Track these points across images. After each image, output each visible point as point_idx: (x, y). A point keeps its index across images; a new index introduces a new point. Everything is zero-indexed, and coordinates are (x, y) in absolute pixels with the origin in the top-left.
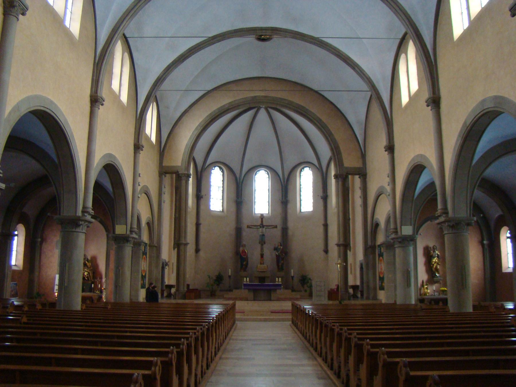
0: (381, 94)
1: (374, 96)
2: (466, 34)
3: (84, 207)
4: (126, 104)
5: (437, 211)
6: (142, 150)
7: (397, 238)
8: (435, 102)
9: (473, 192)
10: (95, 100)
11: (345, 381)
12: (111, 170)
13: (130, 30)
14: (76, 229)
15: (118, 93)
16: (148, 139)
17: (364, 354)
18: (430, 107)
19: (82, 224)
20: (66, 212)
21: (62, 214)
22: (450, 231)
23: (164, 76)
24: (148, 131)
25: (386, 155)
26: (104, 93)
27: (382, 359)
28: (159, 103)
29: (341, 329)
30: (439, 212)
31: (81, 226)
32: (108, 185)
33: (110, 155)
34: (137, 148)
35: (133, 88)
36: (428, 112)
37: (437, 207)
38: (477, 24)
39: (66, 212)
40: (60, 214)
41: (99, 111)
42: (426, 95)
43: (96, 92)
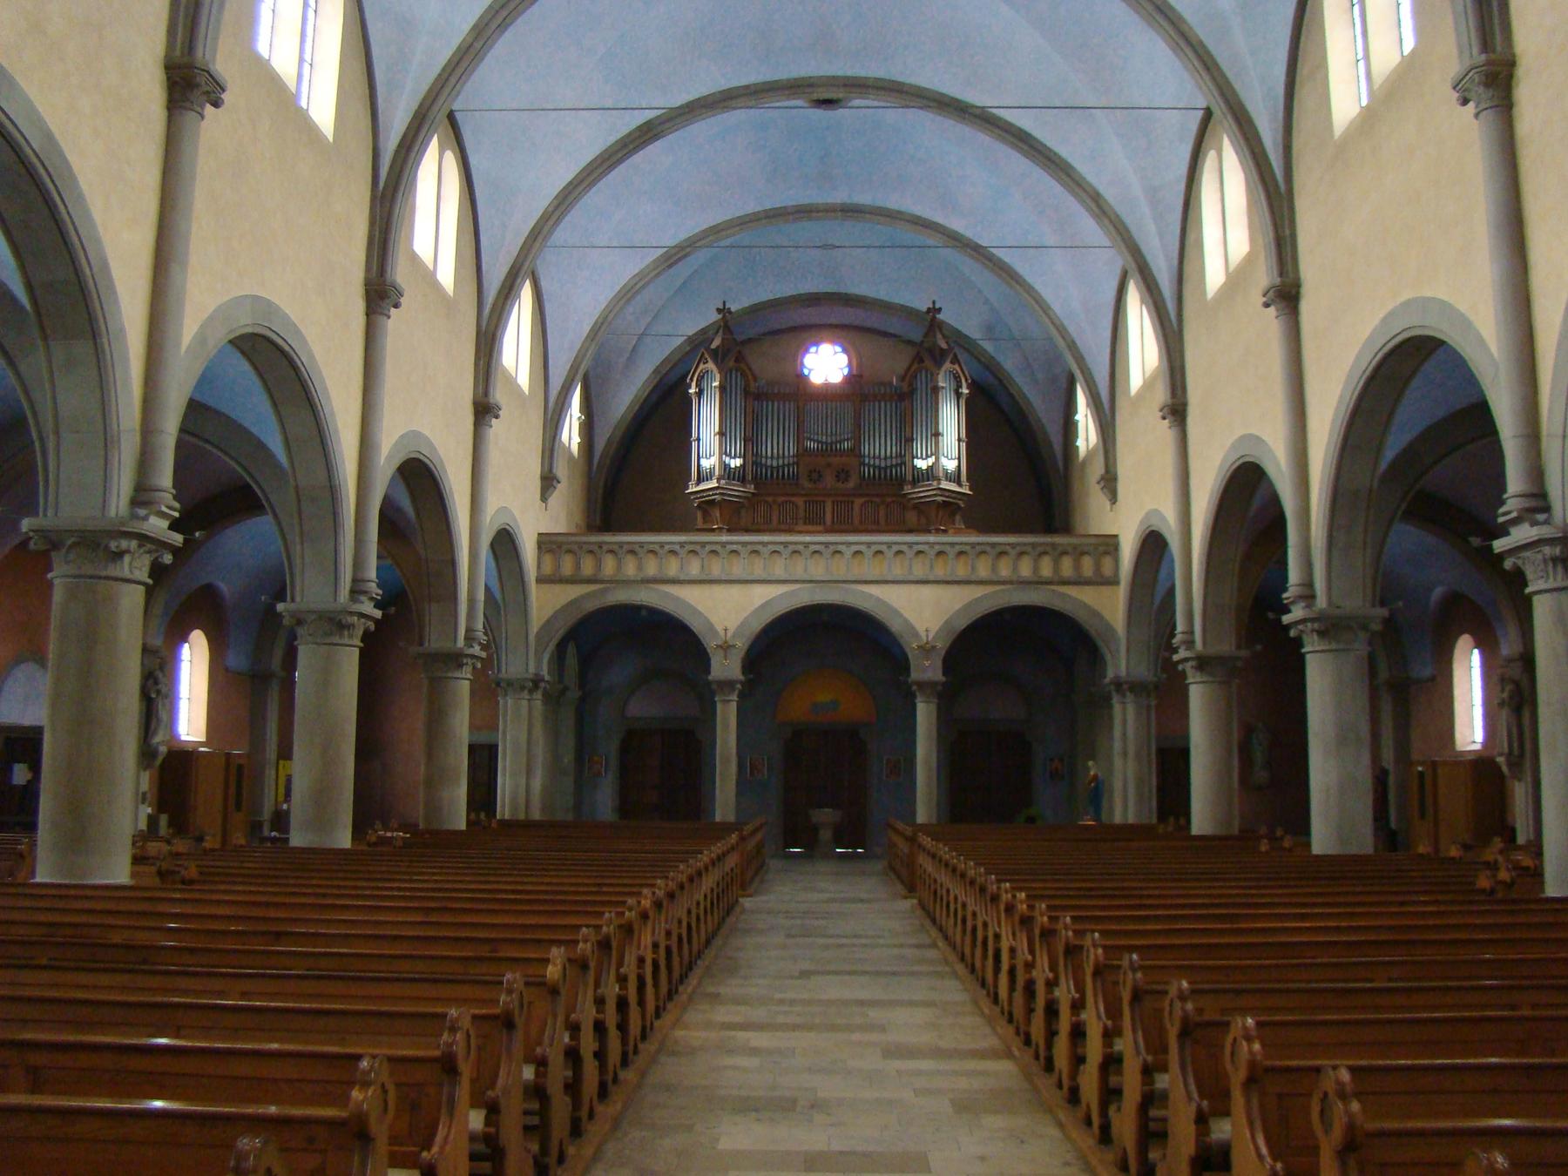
0: (1149, 258)
1: (1132, 266)
2: (1369, 118)
3: (469, 630)
4: (330, 135)
5: (1285, 590)
6: (497, 417)
7: (1312, 620)
8: (1287, 296)
9: (1383, 543)
10: (380, 295)
11: (1042, 1053)
12: (418, 476)
13: (550, 265)
14: (341, 636)
15: (431, 267)
16: (511, 381)
17: (1121, 999)
18: (1272, 309)
19: (128, 551)
20: (435, 641)
21: (298, 599)
22: (1198, 679)
23: (478, 45)
24: (422, 243)
25: (1164, 431)
26: (400, 274)
27: (1092, 957)
28: (544, 284)
29: (1014, 896)
30: (1512, 505)
31: (127, 558)
32: (253, 410)
33: (416, 435)
34: (484, 411)
35: (470, 237)
36: (1464, 130)
37: (1502, 487)
38: (1389, 97)
39: (435, 641)
40: (421, 644)
41: (204, 124)
42: (1264, 277)
43: (486, 394)
